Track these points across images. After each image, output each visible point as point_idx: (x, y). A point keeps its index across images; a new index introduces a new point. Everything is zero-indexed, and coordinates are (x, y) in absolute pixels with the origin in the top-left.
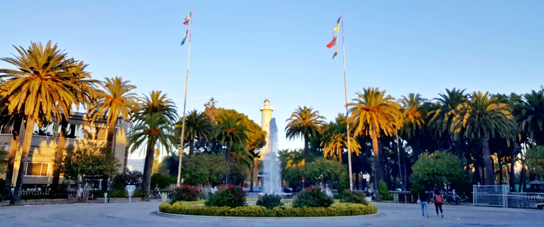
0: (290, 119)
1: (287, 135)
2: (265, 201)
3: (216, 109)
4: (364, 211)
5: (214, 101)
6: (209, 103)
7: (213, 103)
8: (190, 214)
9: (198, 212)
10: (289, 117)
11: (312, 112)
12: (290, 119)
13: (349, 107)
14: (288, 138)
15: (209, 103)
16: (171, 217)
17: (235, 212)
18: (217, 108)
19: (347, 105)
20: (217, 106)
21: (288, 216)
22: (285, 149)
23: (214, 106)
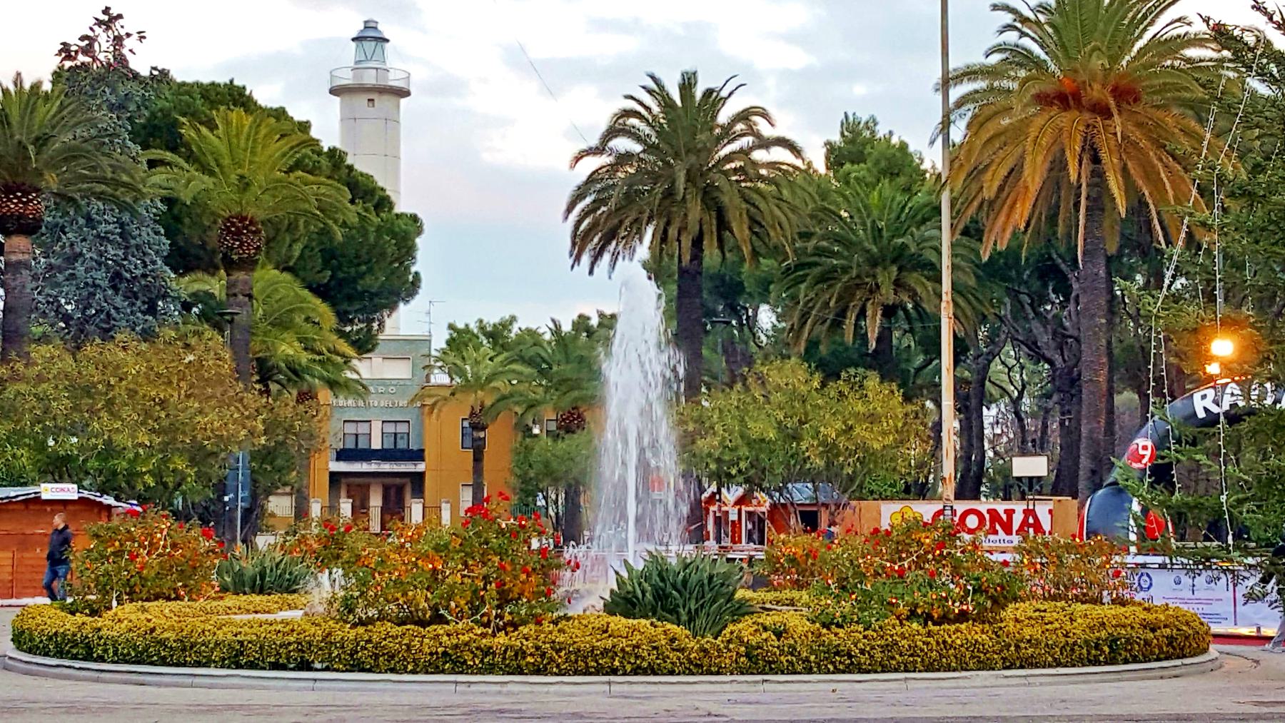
0: (598, 151)
1: (579, 241)
2: (661, 595)
3: (136, 76)
4: (1171, 639)
5: (119, 28)
6: (91, 39)
7: (118, 40)
8: (252, 665)
9: (295, 657)
10: (594, 141)
11: (723, 117)
12: (598, 151)
13: (956, 93)
14: (586, 259)
15: (91, 39)
16: (1147, 675)
17: (520, 653)
18: (144, 72)
19: (946, 82)
20: (141, 63)
21: (809, 671)
22: (492, 319)
23: (122, 60)
